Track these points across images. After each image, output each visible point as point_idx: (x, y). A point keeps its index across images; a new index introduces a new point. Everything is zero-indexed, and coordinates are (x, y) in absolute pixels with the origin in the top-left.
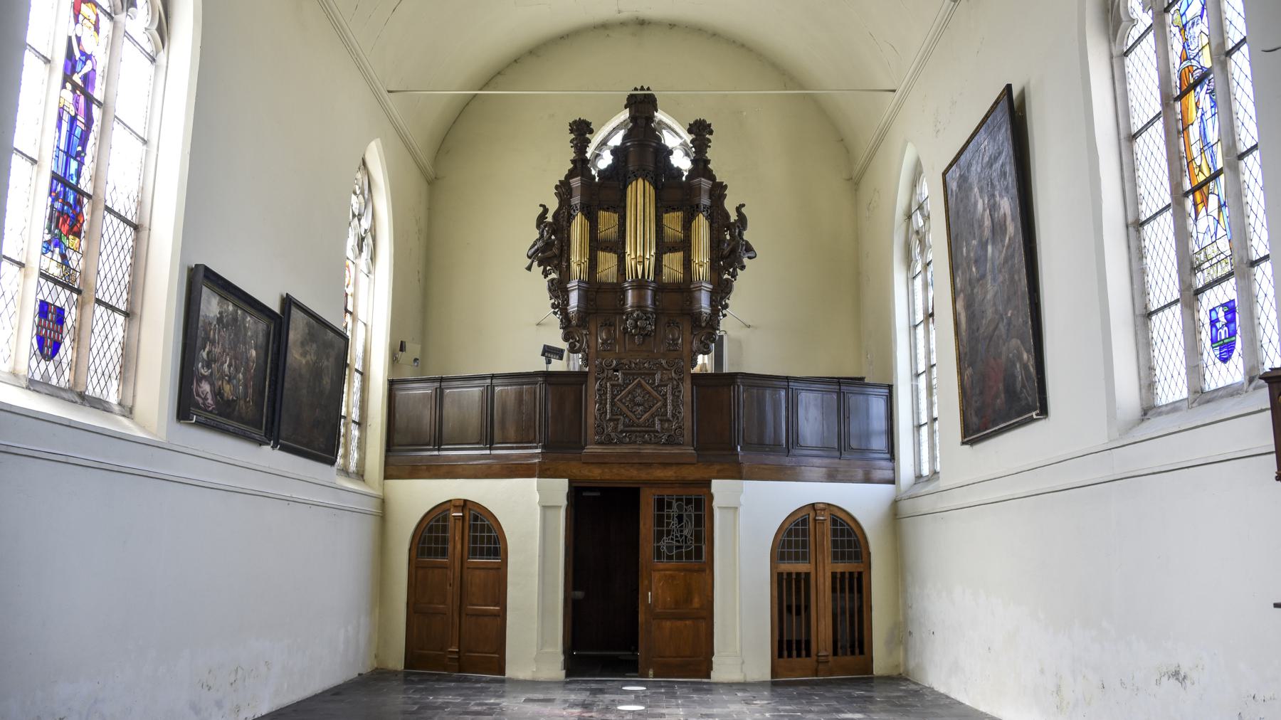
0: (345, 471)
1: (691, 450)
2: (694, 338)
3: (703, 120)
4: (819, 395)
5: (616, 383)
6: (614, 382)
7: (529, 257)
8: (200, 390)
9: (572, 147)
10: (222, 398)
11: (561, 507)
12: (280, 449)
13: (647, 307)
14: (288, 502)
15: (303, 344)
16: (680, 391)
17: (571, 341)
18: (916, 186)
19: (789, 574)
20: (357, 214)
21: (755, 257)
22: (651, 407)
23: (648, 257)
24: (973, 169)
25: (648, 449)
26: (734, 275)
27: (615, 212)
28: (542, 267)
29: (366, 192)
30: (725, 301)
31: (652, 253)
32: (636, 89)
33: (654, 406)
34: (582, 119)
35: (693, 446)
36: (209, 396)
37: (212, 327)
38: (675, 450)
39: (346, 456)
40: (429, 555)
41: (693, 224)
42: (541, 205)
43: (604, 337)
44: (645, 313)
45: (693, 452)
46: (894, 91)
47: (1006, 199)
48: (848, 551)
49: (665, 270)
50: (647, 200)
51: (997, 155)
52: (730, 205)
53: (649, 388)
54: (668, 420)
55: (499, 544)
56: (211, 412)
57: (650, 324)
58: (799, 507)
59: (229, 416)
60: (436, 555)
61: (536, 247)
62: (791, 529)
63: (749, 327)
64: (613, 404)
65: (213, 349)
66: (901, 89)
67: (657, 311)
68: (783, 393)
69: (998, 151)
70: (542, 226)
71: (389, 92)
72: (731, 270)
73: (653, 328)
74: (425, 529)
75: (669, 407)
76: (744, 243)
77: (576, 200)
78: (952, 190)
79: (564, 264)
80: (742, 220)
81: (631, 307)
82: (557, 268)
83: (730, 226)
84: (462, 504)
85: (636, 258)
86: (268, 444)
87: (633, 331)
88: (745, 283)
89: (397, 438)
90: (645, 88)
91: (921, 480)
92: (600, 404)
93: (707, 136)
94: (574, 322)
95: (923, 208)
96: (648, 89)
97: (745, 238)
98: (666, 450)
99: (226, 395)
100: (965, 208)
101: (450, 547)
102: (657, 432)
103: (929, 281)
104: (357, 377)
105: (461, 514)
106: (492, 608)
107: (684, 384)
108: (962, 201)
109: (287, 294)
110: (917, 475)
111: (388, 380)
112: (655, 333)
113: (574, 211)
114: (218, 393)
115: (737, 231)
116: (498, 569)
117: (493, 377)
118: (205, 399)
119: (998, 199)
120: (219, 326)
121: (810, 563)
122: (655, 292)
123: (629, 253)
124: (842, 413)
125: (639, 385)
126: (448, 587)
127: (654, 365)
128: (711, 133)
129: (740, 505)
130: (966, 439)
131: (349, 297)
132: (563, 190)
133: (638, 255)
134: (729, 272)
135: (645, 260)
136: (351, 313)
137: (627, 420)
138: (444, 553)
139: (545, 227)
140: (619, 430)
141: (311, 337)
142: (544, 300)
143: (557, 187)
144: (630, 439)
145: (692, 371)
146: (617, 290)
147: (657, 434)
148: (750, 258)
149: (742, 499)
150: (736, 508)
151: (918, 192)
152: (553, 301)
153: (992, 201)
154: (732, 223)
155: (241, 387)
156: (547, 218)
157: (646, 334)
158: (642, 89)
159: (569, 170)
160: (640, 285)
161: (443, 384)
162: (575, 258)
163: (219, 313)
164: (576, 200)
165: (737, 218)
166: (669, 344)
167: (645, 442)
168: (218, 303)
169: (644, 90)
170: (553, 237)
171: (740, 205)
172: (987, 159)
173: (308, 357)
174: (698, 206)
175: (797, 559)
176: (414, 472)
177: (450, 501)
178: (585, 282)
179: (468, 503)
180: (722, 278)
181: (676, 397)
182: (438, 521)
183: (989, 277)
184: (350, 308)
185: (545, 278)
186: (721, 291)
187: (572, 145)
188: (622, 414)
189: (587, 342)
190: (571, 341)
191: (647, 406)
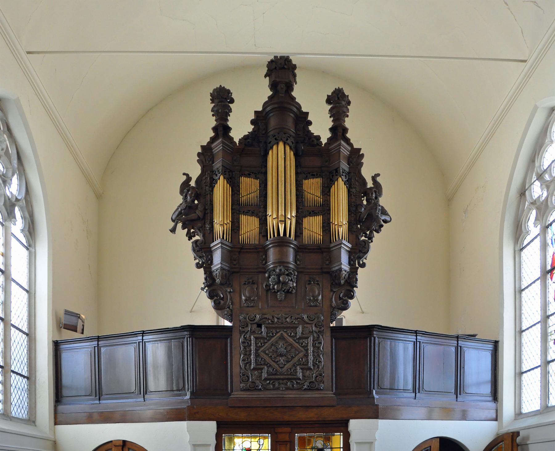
6: (258, 336)
7: (173, 221)
13: (289, 263)
16: (320, 343)
17: (215, 298)
22: (293, 357)
25: (291, 394)
26: (370, 238)
27: (256, 178)
28: (186, 230)
30: (362, 261)
41: (332, 190)
42: (184, 174)
43: (247, 295)
44: (287, 268)
46: (525, 61)
49: (306, 233)
52: (367, 173)
53: (291, 340)
54: (310, 369)
57: (292, 280)
64: (257, 355)
67: (300, 271)
72: (368, 233)
73: (295, 285)
75: (311, 358)
76: (380, 208)
77: (218, 164)
79: (208, 226)
80: (378, 187)
81: (273, 263)
82: (201, 229)
83: (366, 192)
85: (278, 217)
87: (276, 287)
94: (218, 281)
102: (300, 379)
110: (516, 413)
111: (53, 341)
113: (216, 175)
115: (374, 195)
117: (143, 333)
125: (282, 338)
133: (280, 214)
135: (287, 220)
137: (271, 370)
144: (274, 385)
147: (299, 381)
149: (377, 435)
150: (371, 443)
151: (537, 164)
152: (197, 261)
164: (218, 164)
166: (310, 300)
167: (288, 389)
170: (196, 202)
171: (375, 175)
174: (337, 170)
179: (127, 443)
185: (189, 240)
189: (231, 299)
190: (215, 298)
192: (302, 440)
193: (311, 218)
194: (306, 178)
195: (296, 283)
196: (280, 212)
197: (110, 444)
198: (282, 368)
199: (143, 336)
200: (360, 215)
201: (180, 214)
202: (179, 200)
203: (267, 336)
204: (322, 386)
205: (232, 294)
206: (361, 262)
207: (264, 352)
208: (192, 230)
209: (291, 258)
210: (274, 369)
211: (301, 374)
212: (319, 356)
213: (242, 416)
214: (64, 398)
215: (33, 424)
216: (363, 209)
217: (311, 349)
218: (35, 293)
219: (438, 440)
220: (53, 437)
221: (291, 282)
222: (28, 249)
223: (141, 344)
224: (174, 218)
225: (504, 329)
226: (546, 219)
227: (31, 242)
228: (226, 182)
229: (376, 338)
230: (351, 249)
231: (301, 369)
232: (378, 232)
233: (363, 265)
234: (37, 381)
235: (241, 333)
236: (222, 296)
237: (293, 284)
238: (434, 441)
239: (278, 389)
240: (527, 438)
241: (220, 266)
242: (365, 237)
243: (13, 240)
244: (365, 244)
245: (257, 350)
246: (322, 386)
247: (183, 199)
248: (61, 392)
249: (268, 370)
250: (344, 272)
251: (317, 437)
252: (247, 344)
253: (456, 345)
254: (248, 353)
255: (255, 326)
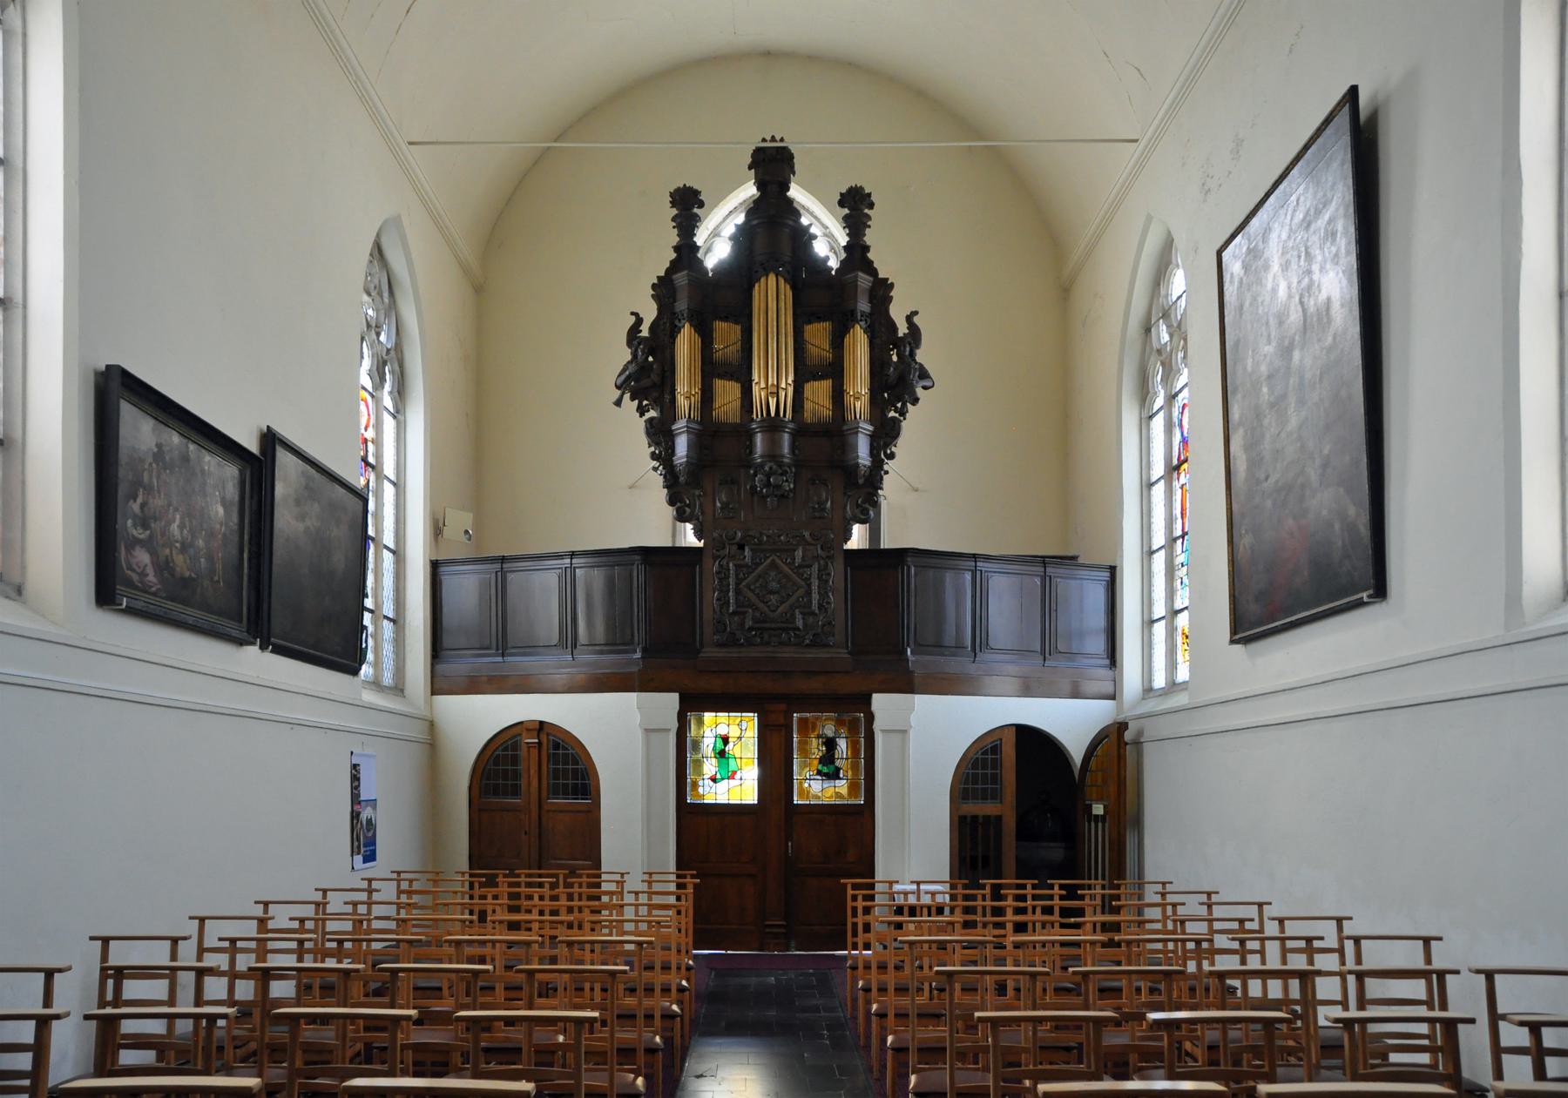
0: (376, 684)
1: (843, 653)
2: (848, 499)
3: (861, 187)
4: (1014, 578)
5: (742, 562)
6: (739, 563)
7: (618, 387)
8: (133, 561)
9: (674, 227)
10: (173, 575)
11: (670, 730)
12: (272, 652)
13: (783, 456)
14: (291, 726)
15: (298, 502)
16: (829, 574)
17: (679, 504)
18: (1159, 285)
19: (975, 818)
20: (374, 325)
21: (933, 386)
22: (789, 596)
23: (783, 385)
24: (1274, 236)
25: (787, 653)
26: (903, 413)
27: (736, 323)
28: (637, 401)
29: (386, 294)
30: (890, 449)
31: (790, 381)
32: (764, 140)
33: (793, 593)
34: (687, 185)
35: (847, 648)
36: (150, 571)
37: (146, 466)
38: (822, 654)
39: (377, 664)
40: (496, 793)
41: (846, 340)
42: (632, 314)
43: (724, 499)
44: (781, 465)
45: (847, 656)
46: (1136, 141)
47: (1332, 274)
48: (978, 769)
49: (808, 406)
50: (782, 304)
51: (1321, 206)
52: (898, 313)
53: (786, 569)
54: (813, 614)
55: (589, 780)
56: (154, 594)
57: (787, 481)
58: (987, 730)
59: (185, 602)
60: (505, 794)
61: (627, 373)
62: (977, 758)
63: (917, 490)
64: (738, 592)
65: (151, 501)
66: (1145, 140)
67: (798, 463)
68: (968, 576)
69: (1323, 201)
70: (635, 343)
71: (411, 143)
72: (899, 405)
73: (792, 486)
74: (1179, 449)
75: (815, 597)
76: (917, 366)
77: (682, 305)
78: (1232, 274)
79: (667, 397)
80: (915, 333)
81: (761, 456)
82: (657, 403)
83: (898, 343)
84: (538, 727)
85: (767, 387)
86: (253, 644)
87: (764, 491)
88: (916, 423)
89: (447, 641)
90: (778, 138)
91: (1151, 694)
92: (721, 591)
93: (866, 211)
94: (682, 479)
95: (1169, 316)
96: (782, 140)
97: (919, 358)
98: (810, 653)
99: (178, 569)
100: (1254, 299)
101: (523, 783)
102: (798, 629)
103: (1176, 420)
104: (388, 557)
105: (537, 741)
106: (581, 862)
107: (834, 564)
108: (1249, 290)
109: (268, 427)
110: (1145, 688)
111: (431, 561)
112: (794, 493)
113: (680, 320)
114: (164, 567)
115: (908, 349)
116: (589, 811)
117: (573, 555)
118: (143, 574)
119: (1316, 277)
120: (158, 465)
121: (1001, 802)
122: (795, 435)
123: (756, 380)
124: (1047, 605)
125: (773, 565)
126: (523, 835)
127: (793, 538)
128: (871, 206)
129: (911, 727)
130: (1237, 637)
131: (370, 444)
132: (664, 289)
133: (770, 383)
134: (896, 407)
135: (780, 391)
136: (373, 467)
137: (758, 614)
138: (516, 791)
139: (639, 344)
140: (747, 627)
141: (308, 493)
142: (642, 448)
143: (654, 286)
144: (762, 638)
145: (845, 547)
146: (742, 432)
147: (797, 633)
148: (925, 388)
149: (913, 719)
150: (904, 732)
151: (1163, 292)
152: (652, 449)
153: (1306, 280)
154: (901, 337)
155: (202, 560)
156: (641, 331)
157: (783, 496)
158: (773, 139)
159: (671, 262)
160: (773, 425)
161: (504, 566)
162: (682, 387)
163: (157, 445)
164: (682, 305)
165: (907, 331)
166: (814, 508)
167: (782, 644)
168: (154, 430)
169: (776, 141)
170: (651, 359)
171: (912, 313)
172: (1301, 216)
173: (308, 523)
174: (853, 313)
175: (984, 798)
176: (473, 686)
177: (521, 723)
178: (697, 422)
179: (545, 725)
180: (886, 416)
181: (823, 582)
182: (506, 749)
183: (1292, 399)
184: (371, 459)
185: (641, 417)
186: (886, 434)
187: (674, 224)
188: (751, 605)
189: (701, 505)
190: (679, 504)
191: (784, 595)
192: (802, 722)
193: (816, 384)
194: (810, 322)
195: (795, 484)
196: (770, 379)
197: (519, 727)
198: (774, 611)
199: (571, 559)
200: (887, 380)
201: (628, 378)
202: (627, 355)
203: (753, 563)
204: (831, 641)
205: (701, 499)
206: (889, 452)
207: (748, 586)
208: (645, 402)
209: (786, 450)
210: (762, 613)
211: (801, 621)
212: (826, 593)
213: (716, 684)
214: (444, 652)
215: (400, 694)
216: (892, 369)
217: (815, 583)
218: (25, 307)
219: (1014, 729)
220: (429, 715)
221: (787, 484)
222: (395, 417)
223: (569, 570)
224: (619, 382)
225: (1124, 548)
226: (1172, 385)
227: (400, 407)
228: (693, 331)
229: (913, 569)
230: (873, 432)
231: (801, 613)
232: (913, 404)
233: (892, 456)
234: (407, 626)
235: (715, 558)
236: (688, 502)
237: (789, 486)
238: (1006, 730)
239: (768, 644)
240: (1140, 733)
241: (685, 460)
242: (896, 412)
243: (385, 413)
244: (894, 423)
245: (738, 584)
246: (831, 641)
247: (631, 353)
248: (441, 643)
249: (753, 616)
250: (862, 468)
251: (825, 720)
252: (723, 574)
253: (1043, 574)
254: (725, 589)
255: (735, 548)
